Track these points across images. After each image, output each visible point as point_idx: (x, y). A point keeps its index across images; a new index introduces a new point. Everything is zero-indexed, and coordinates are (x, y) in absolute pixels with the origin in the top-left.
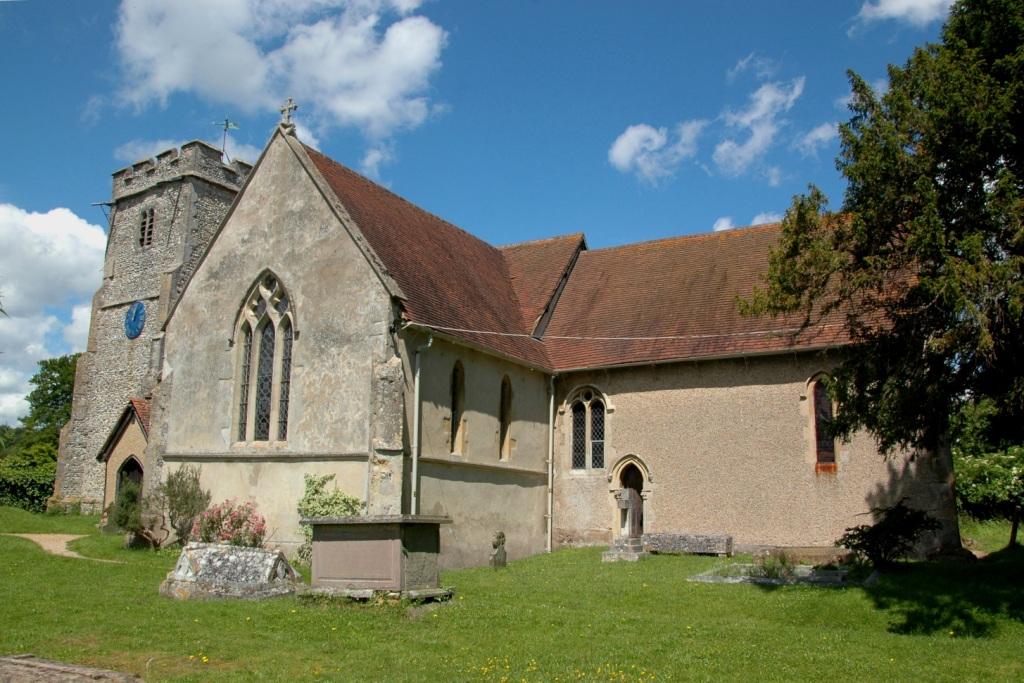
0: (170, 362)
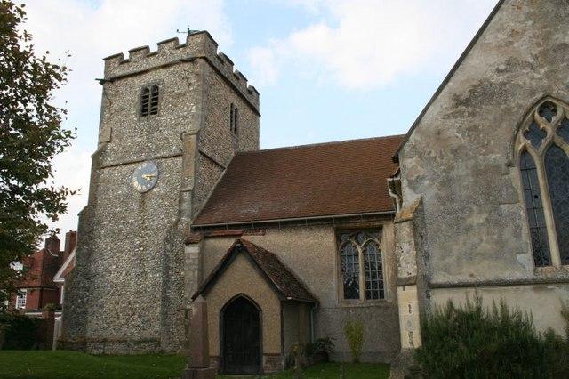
0: (414, 189)
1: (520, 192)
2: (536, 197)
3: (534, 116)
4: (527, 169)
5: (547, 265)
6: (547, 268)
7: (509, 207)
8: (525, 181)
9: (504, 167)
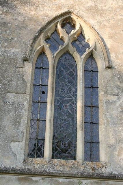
1: (28, 85)
2: (43, 93)
3: (56, 27)
4: (41, 67)
5: (39, 156)
6: (38, 160)
7: (15, 97)
8: (35, 76)
9: (20, 61)
